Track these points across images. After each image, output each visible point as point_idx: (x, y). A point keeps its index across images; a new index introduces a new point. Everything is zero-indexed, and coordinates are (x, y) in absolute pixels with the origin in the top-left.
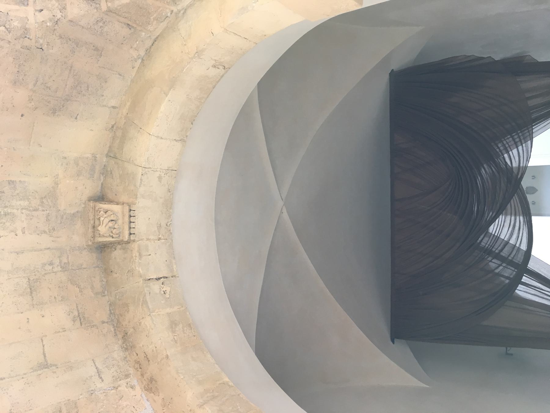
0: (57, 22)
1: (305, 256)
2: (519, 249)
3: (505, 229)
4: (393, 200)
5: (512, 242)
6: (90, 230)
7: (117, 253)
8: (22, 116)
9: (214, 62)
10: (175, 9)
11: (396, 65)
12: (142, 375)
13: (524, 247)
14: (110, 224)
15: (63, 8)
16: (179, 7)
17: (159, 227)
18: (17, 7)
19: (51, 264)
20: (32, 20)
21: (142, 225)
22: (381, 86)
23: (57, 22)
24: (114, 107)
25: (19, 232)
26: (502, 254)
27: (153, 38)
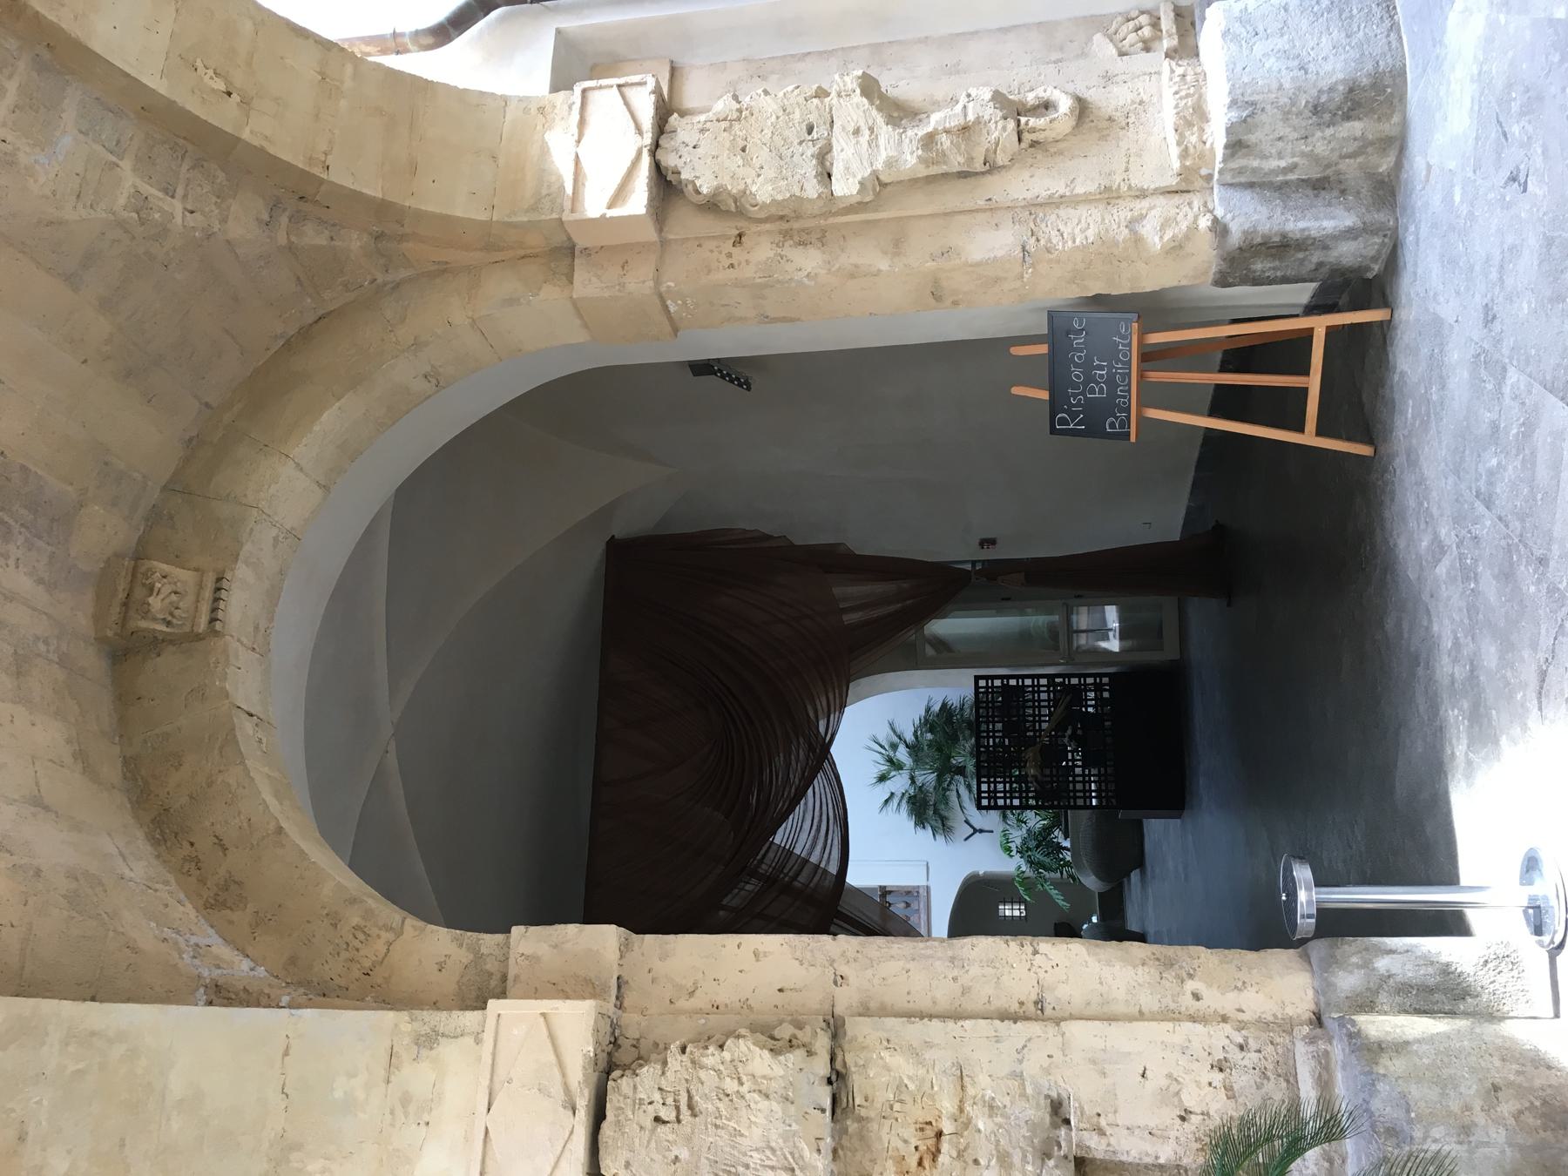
0: (209, 237)
1: (420, 868)
2: (825, 871)
3: (804, 836)
4: (598, 784)
5: (814, 859)
6: (116, 610)
7: (167, 663)
8: (85, 361)
9: (428, 368)
10: (380, 279)
11: (624, 526)
12: (202, 881)
13: (833, 869)
14: (174, 597)
15: (224, 220)
16: (389, 278)
17: (257, 628)
18: (161, 195)
19: (46, 642)
20: (178, 220)
21: (240, 606)
22: (592, 555)
23: (209, 237)
24: (207, 405)
25: (11, 562)
26: (796, 884)
27: (321, 312)
